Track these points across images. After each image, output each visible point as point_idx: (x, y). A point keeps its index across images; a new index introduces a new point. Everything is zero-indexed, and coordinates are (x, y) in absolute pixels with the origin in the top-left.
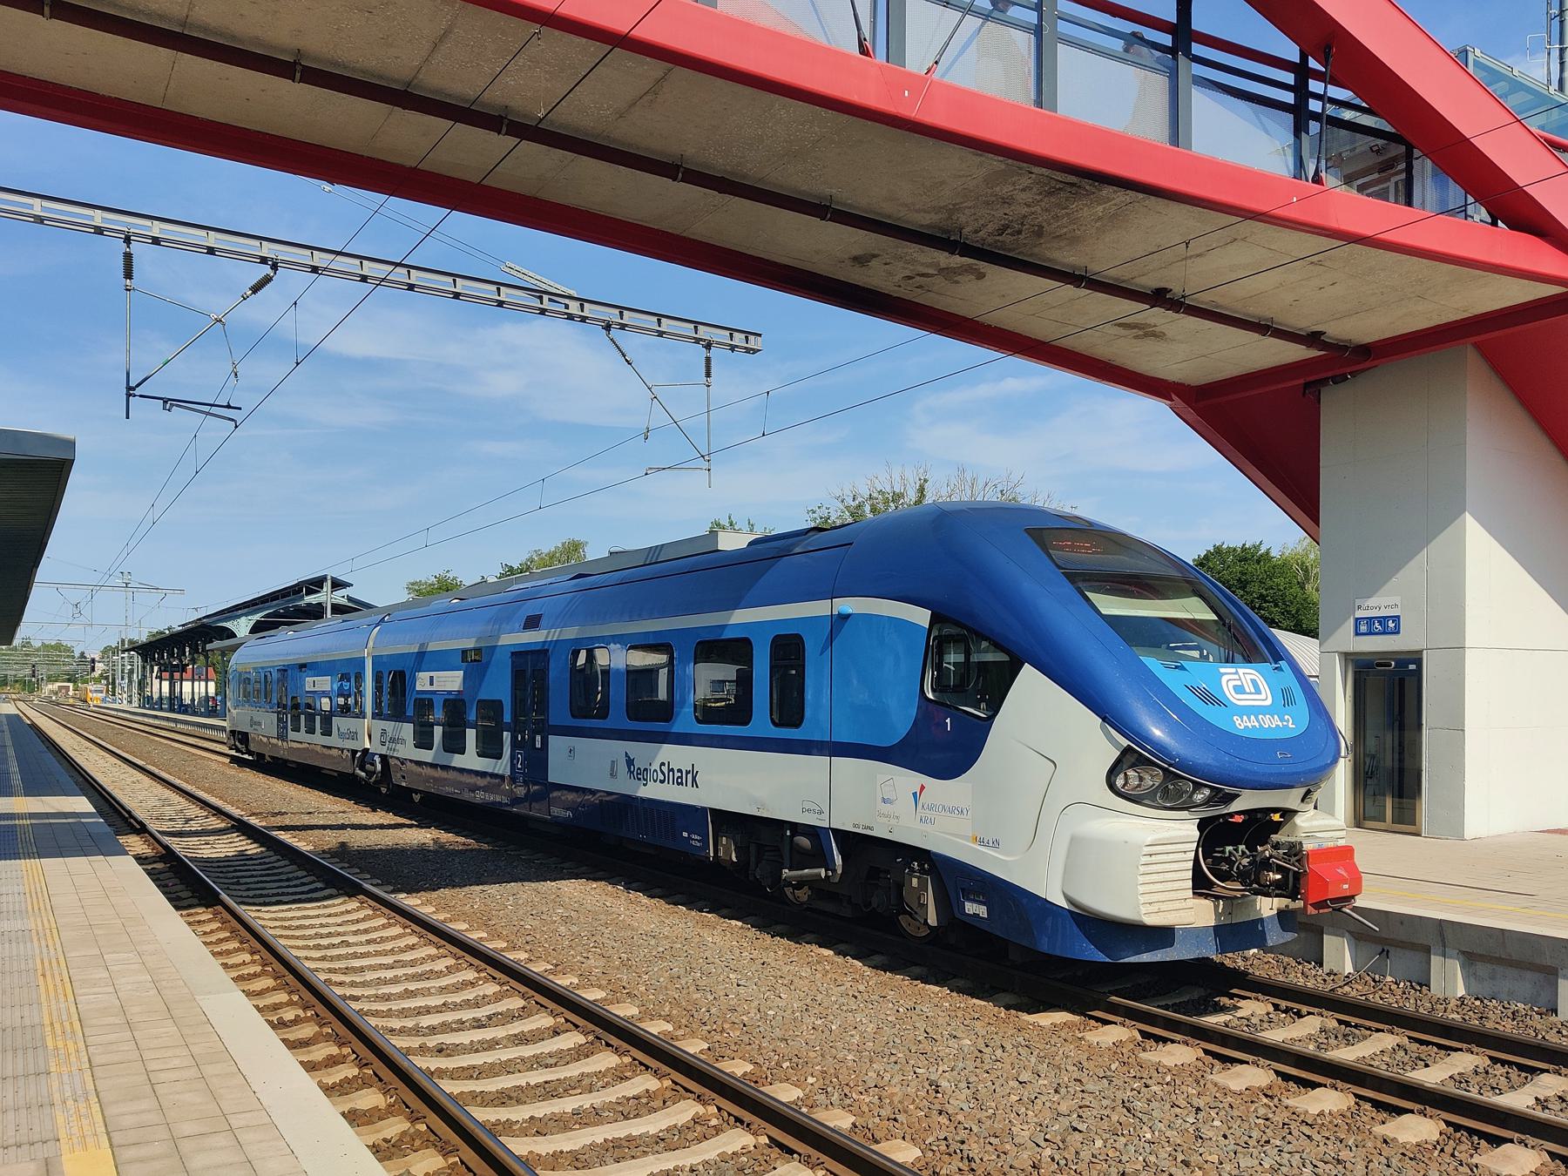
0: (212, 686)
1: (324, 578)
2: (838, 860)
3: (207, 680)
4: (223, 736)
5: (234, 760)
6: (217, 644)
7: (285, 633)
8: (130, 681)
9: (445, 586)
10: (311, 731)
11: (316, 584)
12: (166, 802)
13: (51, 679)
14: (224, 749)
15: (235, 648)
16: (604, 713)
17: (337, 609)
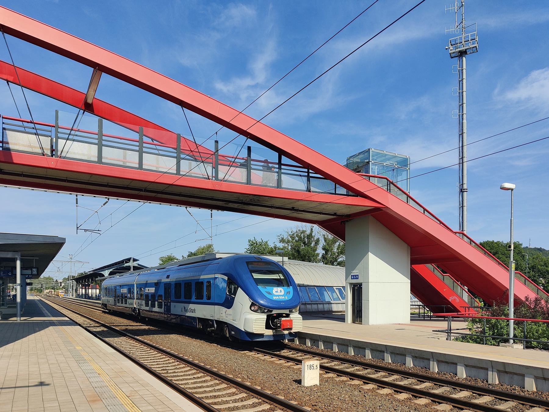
0: (98, 291)
1: (130, 258)
2: (215, 326)
3: (96, 289)
4: (100, 305)
5: (103, 312)
6: (99, 278)
7: (117, 276)
8: (73, 289)
9: (170, 259)
10: (122, 303)
11: (128, 260)
12: (85, 321)
13: (46, 289)
14: (101, 309)
15: (104, 280)
16: (191, 298)
17: (135, 268)
